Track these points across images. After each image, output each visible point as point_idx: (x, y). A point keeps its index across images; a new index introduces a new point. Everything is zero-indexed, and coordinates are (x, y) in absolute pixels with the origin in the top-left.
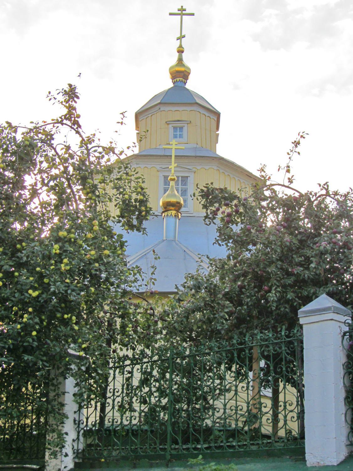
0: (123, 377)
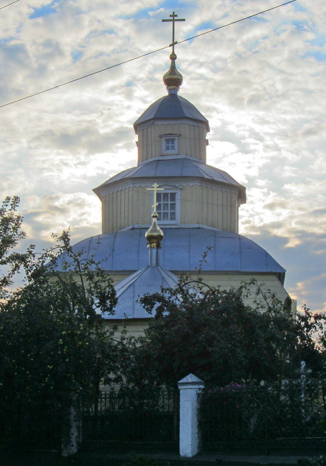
0: (198, 277)
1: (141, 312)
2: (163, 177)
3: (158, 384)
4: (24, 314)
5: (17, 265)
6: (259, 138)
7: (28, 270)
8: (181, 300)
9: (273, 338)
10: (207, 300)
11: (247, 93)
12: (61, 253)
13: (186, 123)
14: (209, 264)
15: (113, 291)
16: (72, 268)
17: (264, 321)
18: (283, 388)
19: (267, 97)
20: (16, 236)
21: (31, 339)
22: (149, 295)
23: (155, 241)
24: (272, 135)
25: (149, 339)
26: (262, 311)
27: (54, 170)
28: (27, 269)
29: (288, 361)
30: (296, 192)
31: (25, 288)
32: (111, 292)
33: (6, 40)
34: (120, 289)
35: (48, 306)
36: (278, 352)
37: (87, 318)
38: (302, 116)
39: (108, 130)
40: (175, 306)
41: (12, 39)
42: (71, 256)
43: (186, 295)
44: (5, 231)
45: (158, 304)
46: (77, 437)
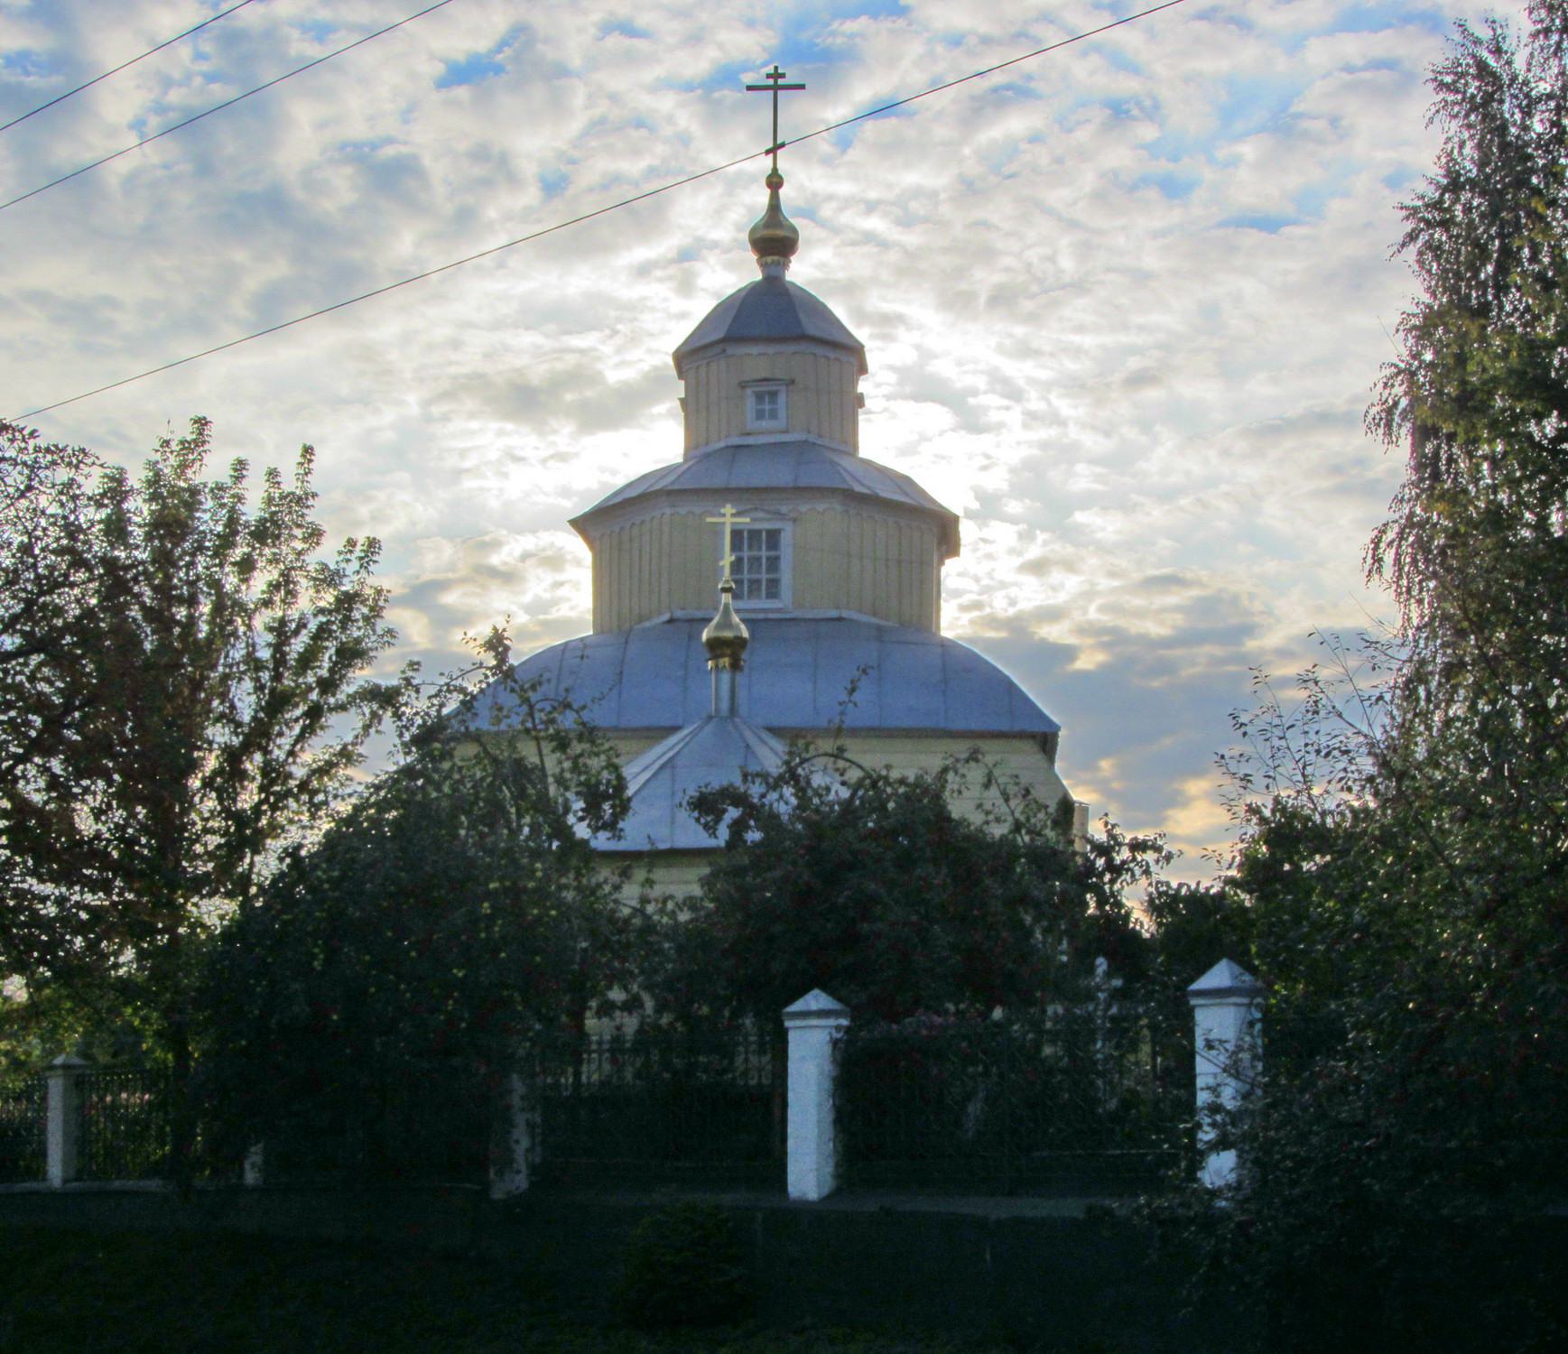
1: (691, 834)
2: (748, 490)
3: (736, 1014)
4: (393, 838)
5: (374, 714)
6: (1013, 394)
7: (405, 726)
8: (794, 801)
9: (1024, 899)
10: (857, 802)
11: (985, 279)
12: (488, 684)
14: (864, 710)
15: (620, 778)
16: (515, 721)
17: (1003, 854)
18: (1049, 1025)
19: (1034, 288)
20: (373, 638)
21: (412, 901)
22: (709, 789)
23: (728, 651)
24: (1046, 387)
25: (712, 900)
26: (998, 831)
27: (489, 474)
28: (399, 723)
29: (1065, 958)
30: (1103, 529)
31: (395, 772)
32: (614, 782)
33: (374, 146)
34: (638, 774)
35: (454, 817)
36: (1039, 936)
37: (554, 847)
38: (1124, 339)
39: (629, 374)
40: (776, 817)
41: (390, 141)
42: (513, 690)
43: (803, 790)
44: (344, 628)
45: (733, 813)
46: (527, 1150)
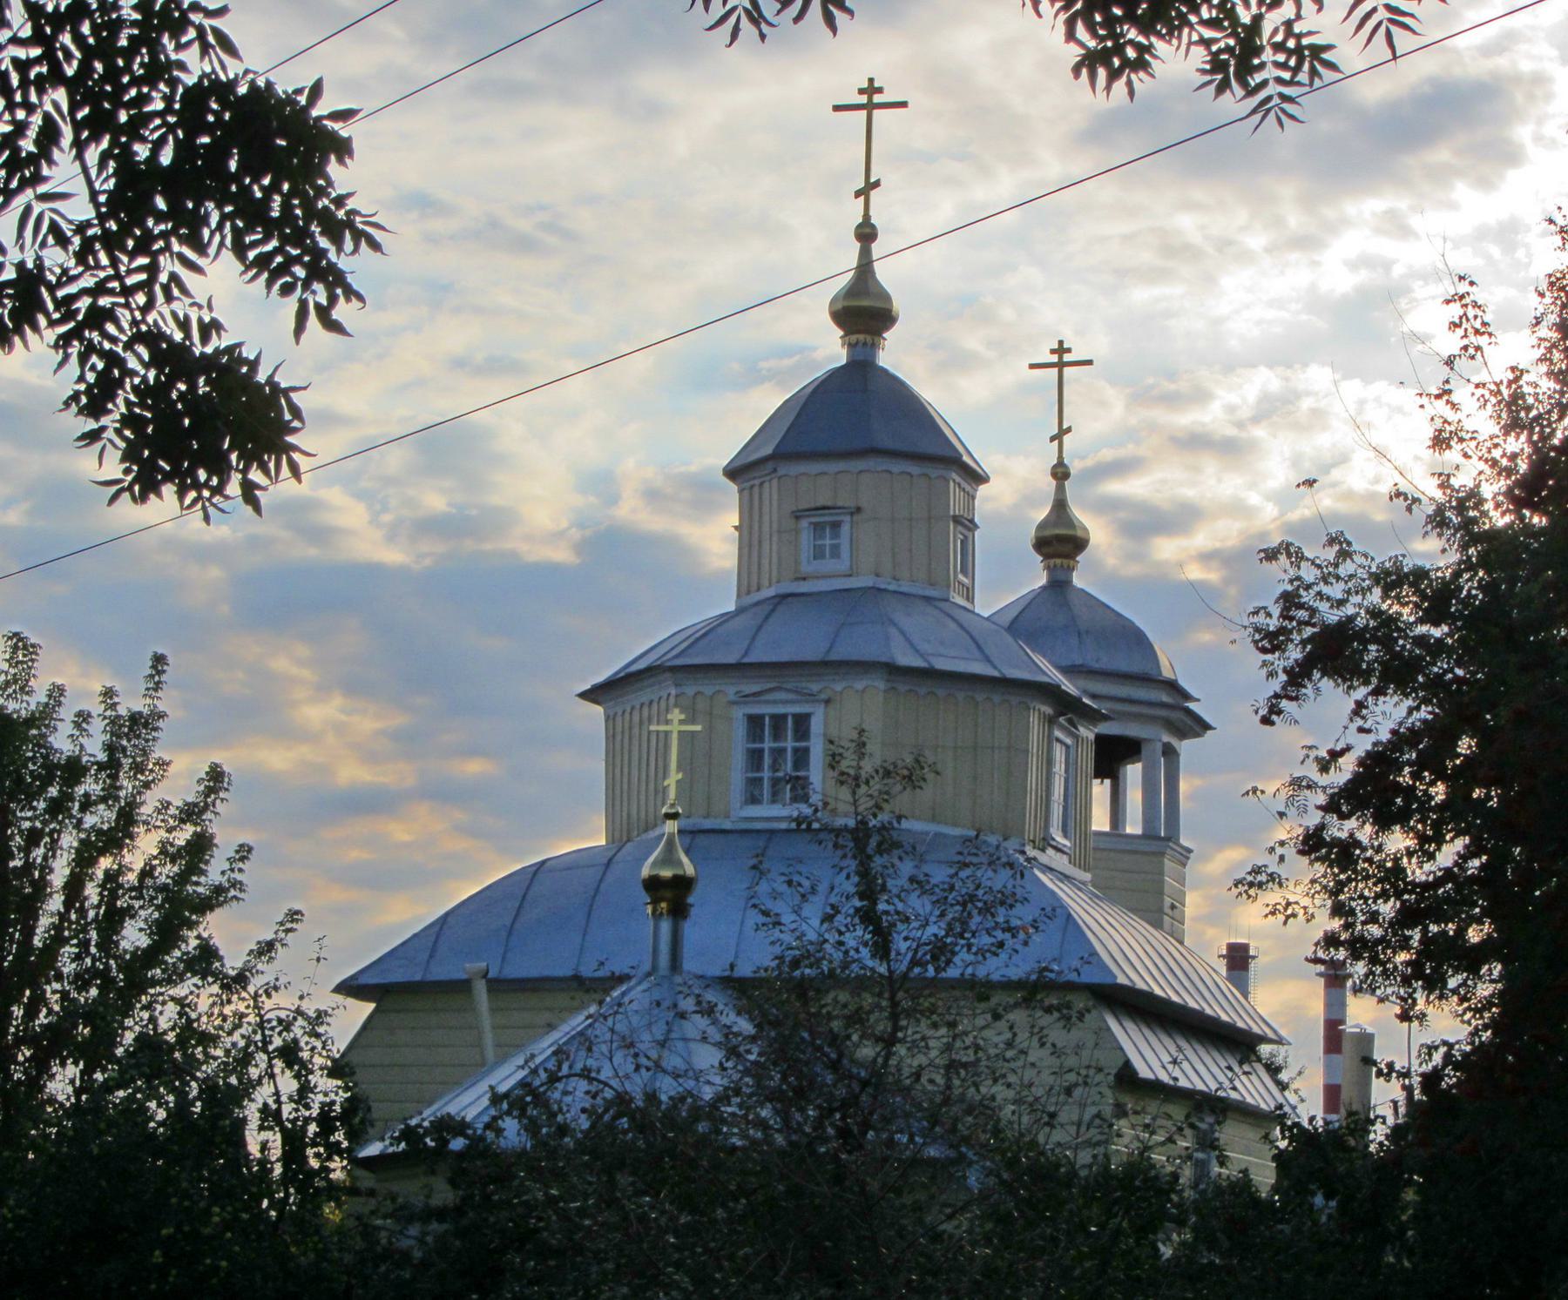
13: (879, 469)
